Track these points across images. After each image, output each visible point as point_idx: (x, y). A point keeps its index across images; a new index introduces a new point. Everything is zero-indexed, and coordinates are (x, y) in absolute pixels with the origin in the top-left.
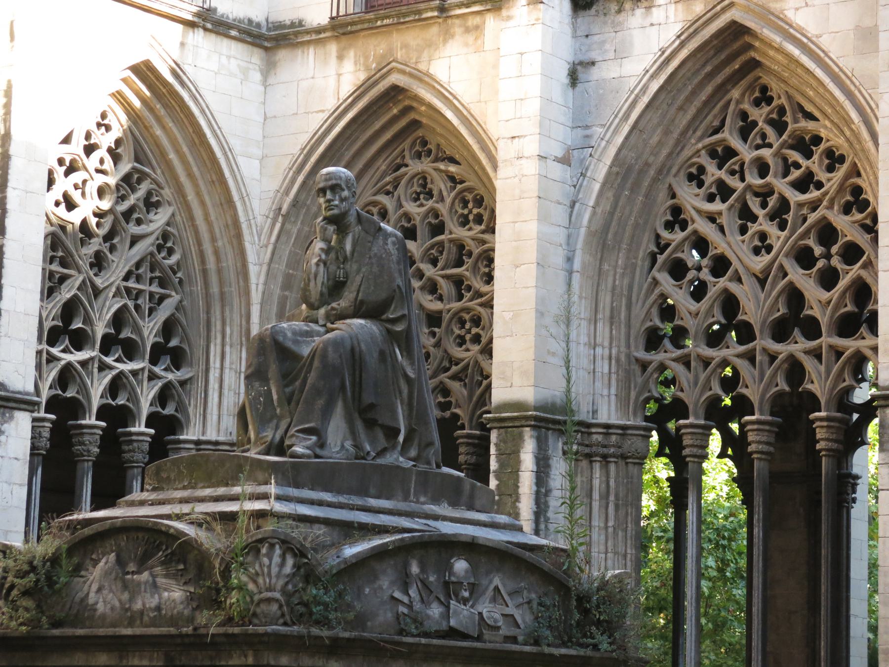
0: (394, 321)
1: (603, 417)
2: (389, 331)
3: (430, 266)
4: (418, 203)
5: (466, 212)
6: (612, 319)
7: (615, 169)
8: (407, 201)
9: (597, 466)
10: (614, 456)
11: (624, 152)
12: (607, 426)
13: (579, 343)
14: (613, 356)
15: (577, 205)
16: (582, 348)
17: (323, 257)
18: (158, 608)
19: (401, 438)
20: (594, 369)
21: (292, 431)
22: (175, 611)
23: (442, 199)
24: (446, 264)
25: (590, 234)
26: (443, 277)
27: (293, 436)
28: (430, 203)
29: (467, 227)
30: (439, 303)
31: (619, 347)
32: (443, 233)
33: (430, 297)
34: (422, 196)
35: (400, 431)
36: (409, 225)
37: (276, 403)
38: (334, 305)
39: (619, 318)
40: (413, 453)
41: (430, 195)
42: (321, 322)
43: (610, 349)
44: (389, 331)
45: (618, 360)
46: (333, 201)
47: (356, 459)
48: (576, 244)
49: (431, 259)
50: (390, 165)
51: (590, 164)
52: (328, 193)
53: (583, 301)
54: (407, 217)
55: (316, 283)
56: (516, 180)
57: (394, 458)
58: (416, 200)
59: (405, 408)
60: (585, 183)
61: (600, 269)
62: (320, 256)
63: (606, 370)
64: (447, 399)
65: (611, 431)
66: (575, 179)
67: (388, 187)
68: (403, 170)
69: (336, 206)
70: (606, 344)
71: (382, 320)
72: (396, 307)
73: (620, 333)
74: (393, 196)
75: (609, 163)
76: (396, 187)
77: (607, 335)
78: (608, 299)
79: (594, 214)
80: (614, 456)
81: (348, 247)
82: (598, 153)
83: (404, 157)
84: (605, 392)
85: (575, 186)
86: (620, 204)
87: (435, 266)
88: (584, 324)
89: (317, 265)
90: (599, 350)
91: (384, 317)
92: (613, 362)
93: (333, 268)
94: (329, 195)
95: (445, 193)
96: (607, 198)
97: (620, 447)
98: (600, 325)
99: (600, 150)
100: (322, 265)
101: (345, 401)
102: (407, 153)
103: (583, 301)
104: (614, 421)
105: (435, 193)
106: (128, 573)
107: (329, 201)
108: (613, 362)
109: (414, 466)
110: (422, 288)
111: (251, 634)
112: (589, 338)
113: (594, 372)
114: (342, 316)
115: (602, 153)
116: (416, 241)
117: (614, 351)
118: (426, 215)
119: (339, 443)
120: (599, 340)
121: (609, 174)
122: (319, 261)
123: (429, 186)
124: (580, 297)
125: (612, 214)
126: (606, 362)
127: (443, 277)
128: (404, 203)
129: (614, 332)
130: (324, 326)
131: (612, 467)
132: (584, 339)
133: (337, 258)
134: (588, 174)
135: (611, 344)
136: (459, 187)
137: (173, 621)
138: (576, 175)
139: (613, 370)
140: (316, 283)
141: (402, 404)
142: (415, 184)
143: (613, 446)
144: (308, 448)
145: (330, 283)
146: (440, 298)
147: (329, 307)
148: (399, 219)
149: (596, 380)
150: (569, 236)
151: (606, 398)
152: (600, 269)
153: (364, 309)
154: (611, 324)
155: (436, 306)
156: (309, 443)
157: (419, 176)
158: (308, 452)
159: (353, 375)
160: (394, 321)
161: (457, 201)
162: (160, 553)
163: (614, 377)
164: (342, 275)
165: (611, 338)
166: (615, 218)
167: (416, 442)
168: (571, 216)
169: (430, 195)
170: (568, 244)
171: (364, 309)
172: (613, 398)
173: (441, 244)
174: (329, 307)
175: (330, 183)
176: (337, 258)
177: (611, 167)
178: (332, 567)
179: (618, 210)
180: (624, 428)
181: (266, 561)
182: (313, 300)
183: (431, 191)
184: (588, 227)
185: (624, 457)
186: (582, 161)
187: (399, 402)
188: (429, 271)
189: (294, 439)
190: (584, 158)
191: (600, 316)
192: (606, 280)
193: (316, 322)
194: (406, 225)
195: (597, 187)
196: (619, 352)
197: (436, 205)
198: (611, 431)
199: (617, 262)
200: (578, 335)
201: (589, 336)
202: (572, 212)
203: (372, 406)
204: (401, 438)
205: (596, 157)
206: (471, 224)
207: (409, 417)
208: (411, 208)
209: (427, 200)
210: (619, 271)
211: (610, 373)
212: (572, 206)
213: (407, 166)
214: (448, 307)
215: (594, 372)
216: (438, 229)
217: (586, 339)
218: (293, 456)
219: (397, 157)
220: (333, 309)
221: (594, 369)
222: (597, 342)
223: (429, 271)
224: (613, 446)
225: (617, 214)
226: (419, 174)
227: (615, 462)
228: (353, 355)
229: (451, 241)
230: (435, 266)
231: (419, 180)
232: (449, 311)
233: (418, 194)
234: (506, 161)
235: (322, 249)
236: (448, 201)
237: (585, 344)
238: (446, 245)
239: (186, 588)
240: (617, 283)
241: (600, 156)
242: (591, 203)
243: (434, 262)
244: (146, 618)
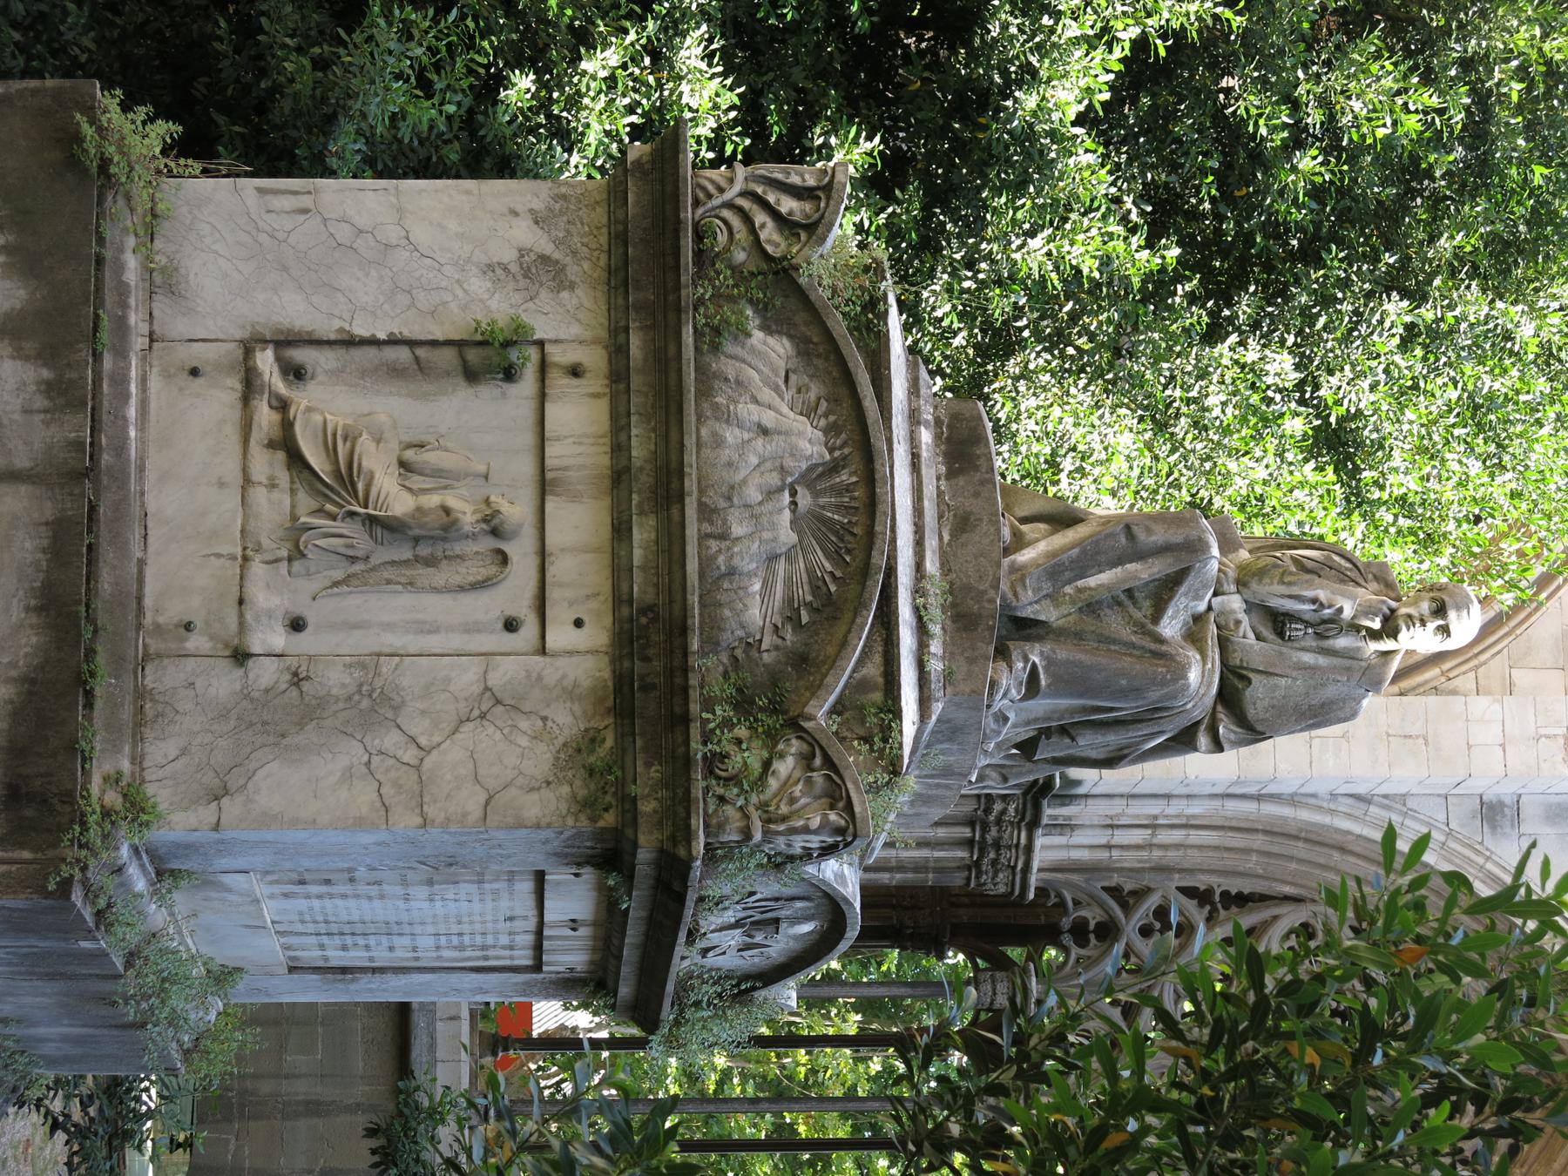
2: (1197, 724)
9: (966, 832)
12: (1029, 849)
18: (732, 572)
22: (727, 613)
37: (1080, 583)
62: (1330, 607)
64: (1092, 936)
89: (1314, 601)
91: (1219, 708)
106: (793, 494)
111: (689, 826)
130: (1210, 608)
131: (961, 854)
137: (713, 625)
153: (1236, 681)
162: (827, 565)
178: (811, 718)
181: (815, 822)
182: (1254, 585)
193: (1215, 594)
220: (1238, 623)
235: (1340, 610)
239: (769, 629)
244: (714, 545)
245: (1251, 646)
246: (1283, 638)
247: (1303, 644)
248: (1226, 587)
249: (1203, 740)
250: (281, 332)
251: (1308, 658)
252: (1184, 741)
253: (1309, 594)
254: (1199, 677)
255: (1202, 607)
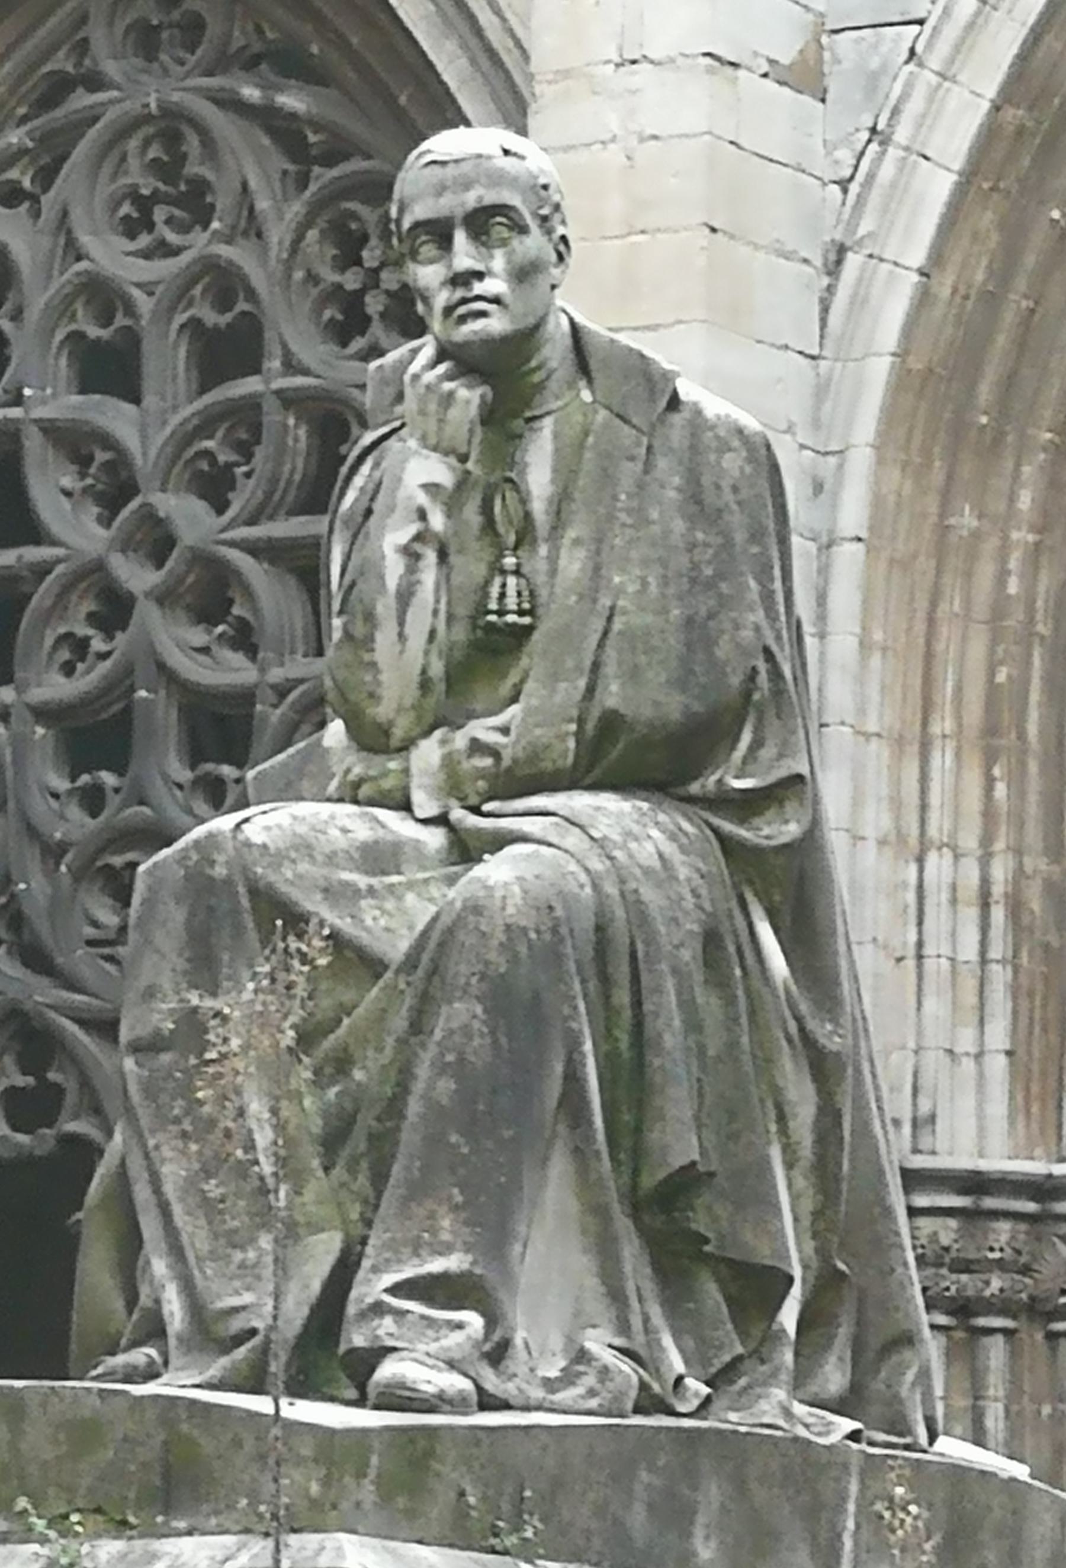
0: (749, 805)
1: (956, 1153)
2: (728, 845)
3: (199, 507)
4: (144, 240)
5: (351, 281)
6: (994, 739)
7: (1012, 115)
8: (95, 233)
10: (1002, 1306)
11: (1051, 43)
12: (975, 1183)
13: (857, 838)
14: (998, 890)
15: (853, 261)
16: (869, 853)
17: (437, 521)
19: (789, 1316)
20: (920, 944)
21: (372, 1286)
23: (250, 227)
24: (269, 495)
25: (902, 381)
26: (253, 548)
27: (378, 1309)
28: (199, 243)
29: (358, 344)
30: (237, 659)
31: (1018, 852)
32: (256, 369)
33: (198, 636)
34: (160, 214)
35: (790, 1280)
36: (104, 334)
38: (482, 729)
39: (1022, 736)
40: (834, 1377)
41: (196, 205)
42: (425, 804)
43: (985, 860)
44: (728, 845)
45: (1015, 906)
46: (480, 276)
47: (638, 1410)
48: (849, 423)
49: (199, 475)
50: (21, 78)
51: (909, 86)
52: (460, 238)
53: (875, 660)
54: (102, 295)
55: (401, 636)
56: (614, 154)
57: (771, 1407)
58: (130, 229)
59: (800, 1183)
60: (887, 171)
61: (943, 530)
62: (422, 515)
63: (969, 951)
65: (990, 1203)
66: (846, 156)
67: (13, 174)
68: (81, 100)
69: (496, 300)
70: (970, 841)
71: (691, 800)
72: (757, 744)
73: (1022, 795)
74: (36, 214)
75: (991, 90)
76: (47, 176)
77: (973, 802)
78: (978, 650)
79: (923, 299)
80: (1002, 1306)
81: (539, 477)
82: (944, 47)
83: (83, 47)
84: (966, 1041)
85: (844, 185)
86: (1030, 260)
87: (221, 508)
88: (878, 752)
89: (410, 554)
90: (938, 866)
92: (998, 914)
93: (471, 567)
94: (464, 254)
95: (263, 204)
96: (975, 237)
97: (1026, 1270)
98: (942, 761)
99: (951, 33)
100: (431, 556)
101: (581, 1154)
102: (97, 34)
103: (875, 660)
104: (998, 1162)
105: (223, 201)
107: (462, 279)
108: (998, 914)
109: (854, 1436)
110: (164, 597)
112: (897, 818)
113: (920, 957)
114: (523, 779)
115: (957, 48)
116: (136, 400)
117: (1000, 872)
118: (181, 293)
119: (556, 1342)
120: (938, 825)
121: (989, 134)
122: (418, 538)
123: (194, 168)
124: (865, 645)
125: (992, 300)
126: (971, 914)
127: (253, 548)
128: (85, 240)
129: (1001, 790)
130: (441, 820)
131: (996, 1351)
132: (876, 820)
133: (489, 524)
134: (901, 135)
135: (987, 840)
136: (323, 176)
138: (846, 140)
139: (996, 952)
140: (401, 636)
141: (789, 1165)
142: (134, 163)
143: (1000, 1265)
144: (452, 1365)
145: (461, 633)
146: (245, 639)
147: (460, 740)
148: (64, 308)
149: (929, 987)
150: (821, 390)
151: (968, 1065)
152: (943, 530)
153: (615, 752)
154: (990, 758)
155: (233, 671)
156: (455, 1338)
157: (149, 130)
158: (456, 1383)
159: (604, 1035)
160: (749, 805)
161: (312, 235)
163: (1000, 976)
164: (511, 602)
165: (989, 814)
166: (1009, 317)
167: (844, 1333)
168: (825, 310)
169: (196, 205)
170: (816, 424)
171: (615, 752)
172: (998, 1065)
173: (246, 418)
174: (460, 740)
175: (471, 199)
176: (489, 524)
177: (996, 108)
179: (1021, 283)
180: (1043, 1189)
182: (383, 711)
183: (200, 187)
184: (902, 354)
185: (1038, 1310)
186: (873, 81)
187: (775, 1153)
188: (188, 516)
189: (388, 1323)
190: (884, 68)
191: (943, 724)
192: (968, 575)
193: (405, 806)
194: (94, 332)
195: (938, 187)
196: (1019, 874)
197: (225, 251)
198: (990, 1203)
199: (1012, 498)
200: (857, 803)
201: (896, 803)
202: (830, 289)
203: (687, 1181)
204: (789, 1316)
205: (935, 62)
206: (377, 331)
207: (821, 1223)
208: (111, 255)
209: (185, 229)
210: (1022, 536)
211: (984, 960)
212: (834, 266)
213: (95, 82)
214: (276, 674)
215: (920, 957)
216: (228, 349)
217: (886, 822)
218: (399, 1398)
219: (54, 48)
220: (476, 747)
221: (920, 944)
222: (933, 831)
223: (188, 516)
224: (1000, 1265)
225: (1015, 304)
226: (147, 119)
227: (1007, 1332)
228: (606, 948)
229: (288, 400)
230: (221, 508)
231: (146, 143)
232: (282, 691)
233: (145, 204)
234: (566, 74)
236: (278, 235)
237: (882, 842)
238: (272, 415)
240: (1013, 587)
241: (951, 61)
242: (917, 257)
243: (215, 488)
245: (528, 712)
246: (529, 629)
247: (541, 579)
248: (387, 784)
249: (780, 829)
250: (178, 275)
251: (573, 564)
252: (793, 887)
253: (394, 569)
254: (600, 840)
255: (435, 839)
